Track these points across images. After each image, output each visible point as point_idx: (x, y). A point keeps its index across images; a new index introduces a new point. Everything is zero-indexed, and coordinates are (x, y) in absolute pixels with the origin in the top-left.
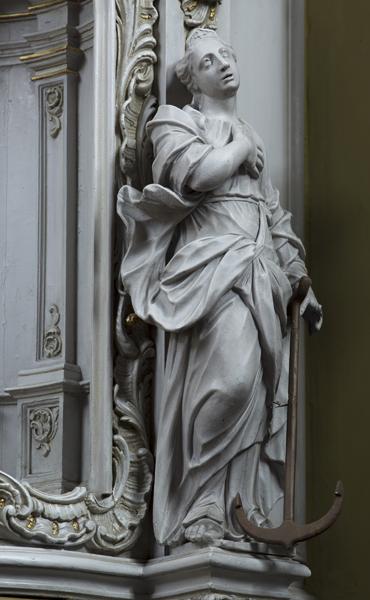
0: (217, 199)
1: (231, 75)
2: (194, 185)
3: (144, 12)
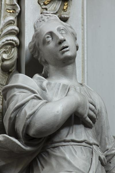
0: (57, 144)
1: (67, 47)
2: (32, 132)
3: (9, 7)
